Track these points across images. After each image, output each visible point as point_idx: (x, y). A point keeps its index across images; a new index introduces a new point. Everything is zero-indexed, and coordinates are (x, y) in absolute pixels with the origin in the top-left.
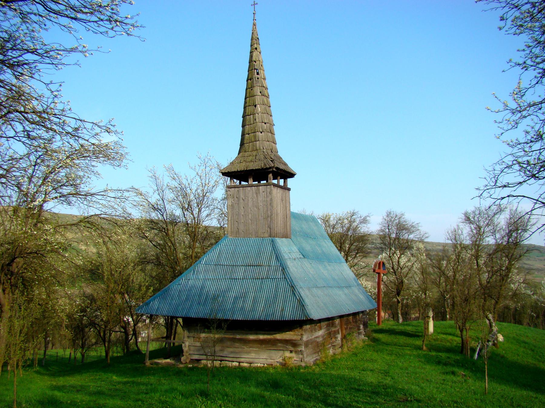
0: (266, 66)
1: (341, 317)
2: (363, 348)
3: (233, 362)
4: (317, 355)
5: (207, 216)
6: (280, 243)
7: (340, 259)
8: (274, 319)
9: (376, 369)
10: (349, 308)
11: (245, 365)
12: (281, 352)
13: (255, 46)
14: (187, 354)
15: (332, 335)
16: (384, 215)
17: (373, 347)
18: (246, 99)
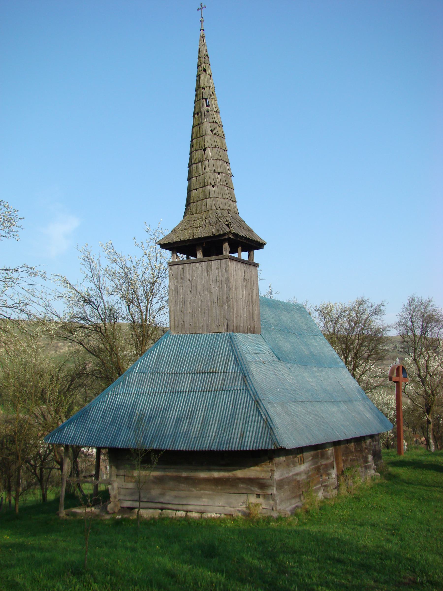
1: (336, 444)
2: (372, 488)
3: (179, 511)
4: (298, 500)
5: (159, 310)
8: (230, 449)
11: (195, 515)
12: (245, 496)
13: (204, 66)
15: (322, 471)
16: (405, 304)
17: (387, 487)
18: (192, 141)
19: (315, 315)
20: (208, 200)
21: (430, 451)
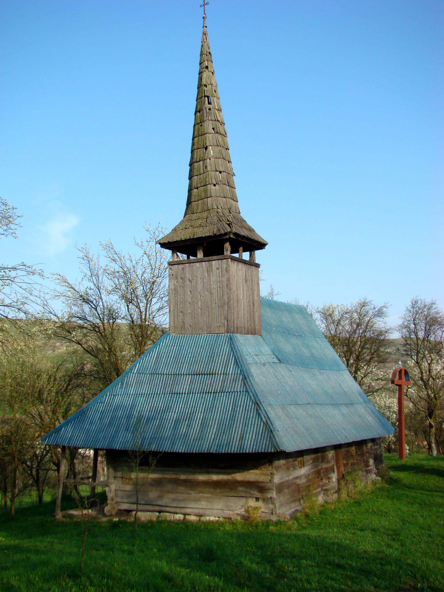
0: (220, 92)
1: (337, 447)
2: (372, 492)
3: (177, 513)
4: (297, 503)
5: (159, 310)
6: (242, 341)
7: (338, 365)
9: (382, 527)
10: (346, 434)
11: (193, 518)
13: (206, 63)
14: (114, 502)
15: (322, 475)
16: (408, 306)
18: (193, 139)
19: (317, 316)
21: (432, 455)
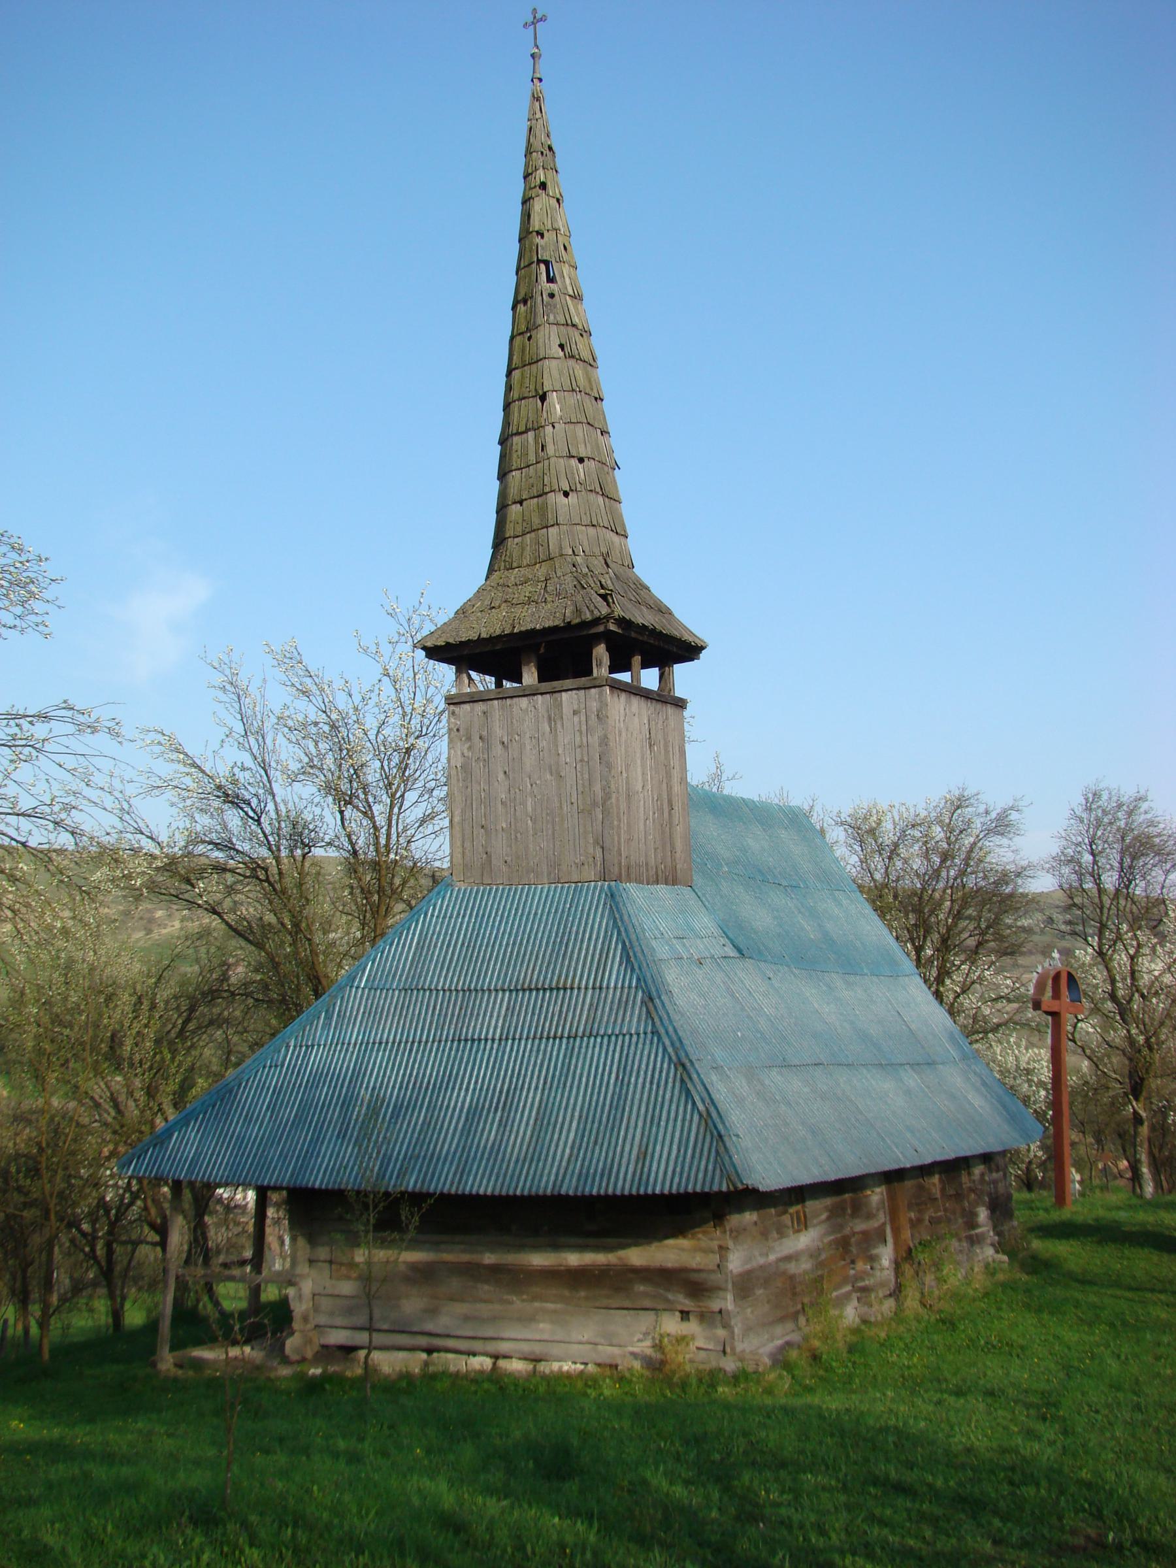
1: (893, 1177)
2: (986, 1295)
3: (474, 1355)
4: (790, 1325)
5: (423, 822)
8: (610, 1191)
9: (1013, 1384)
11: (516, 1366)
12: (650, 1317)
13: (541, 175)
15: (854, 1250)
16: (1075, 805)
17: (1028, 1291)
18: (509, 374)
19: (837, 835)
20: (553, 531)
21: (1141, 1197)
